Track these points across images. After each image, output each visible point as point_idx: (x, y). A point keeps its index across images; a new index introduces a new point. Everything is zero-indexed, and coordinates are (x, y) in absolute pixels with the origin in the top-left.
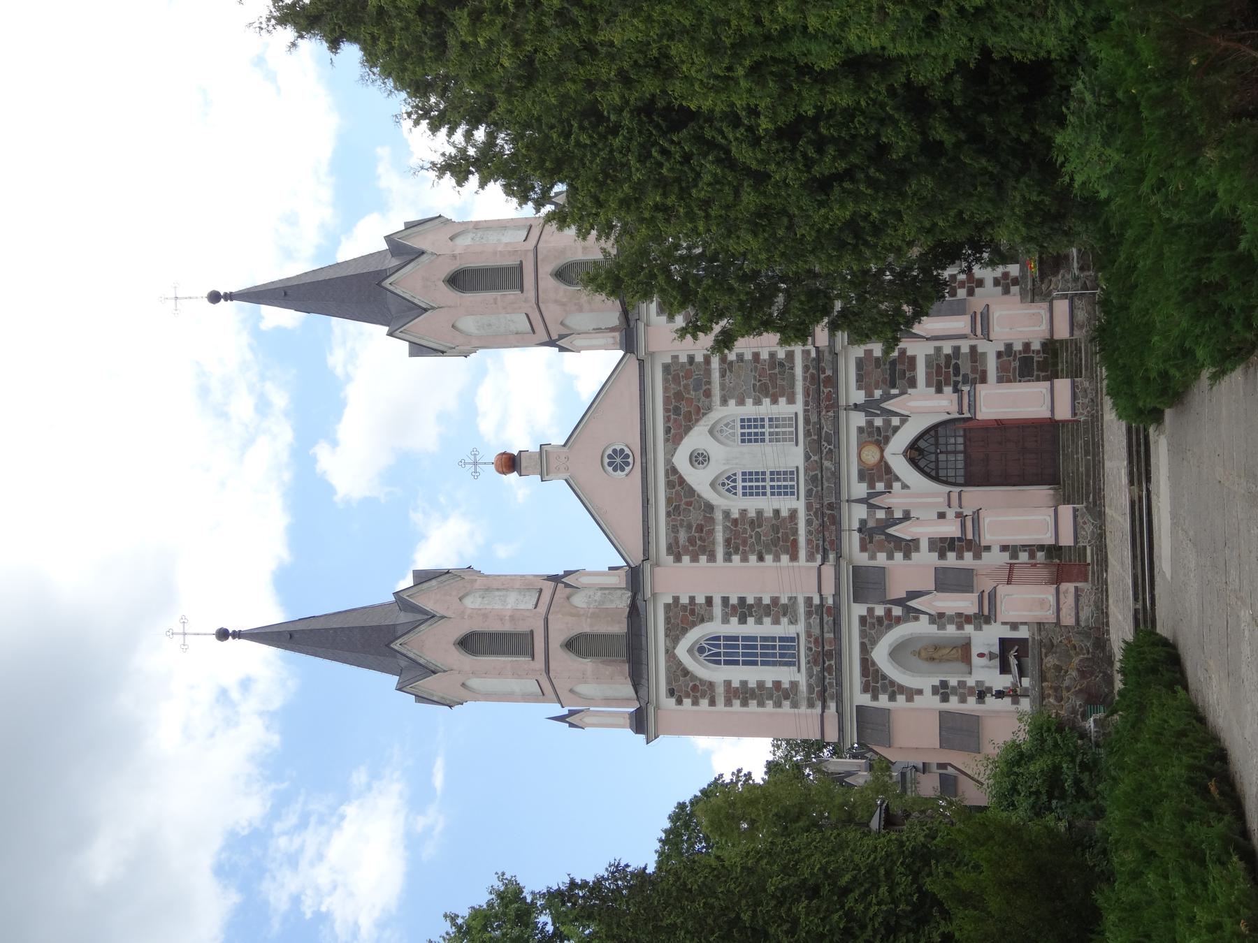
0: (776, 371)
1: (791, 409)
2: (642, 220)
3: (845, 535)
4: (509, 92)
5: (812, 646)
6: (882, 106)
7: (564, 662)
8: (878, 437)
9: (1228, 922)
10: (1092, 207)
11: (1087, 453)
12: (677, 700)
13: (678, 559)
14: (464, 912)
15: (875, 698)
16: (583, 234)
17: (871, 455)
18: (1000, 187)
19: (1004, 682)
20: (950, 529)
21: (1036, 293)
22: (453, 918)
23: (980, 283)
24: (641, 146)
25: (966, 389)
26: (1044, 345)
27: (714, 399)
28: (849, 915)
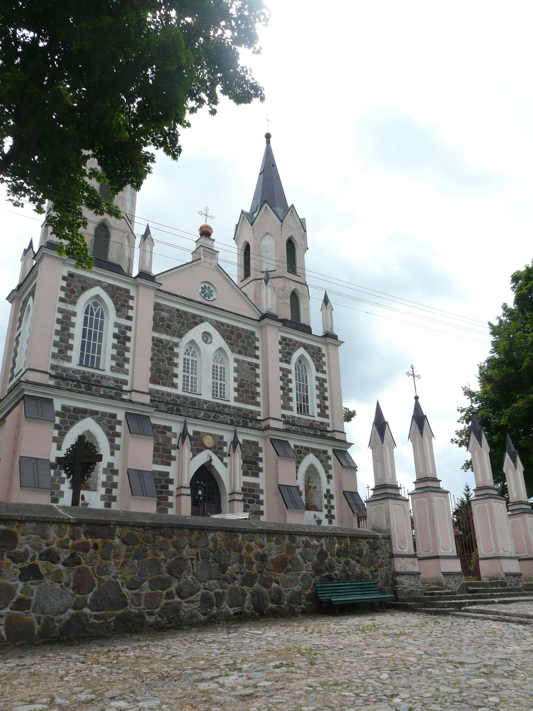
0: (250, 394)
5: (95, 378)
12: (66, 277)
27: (238, 355)
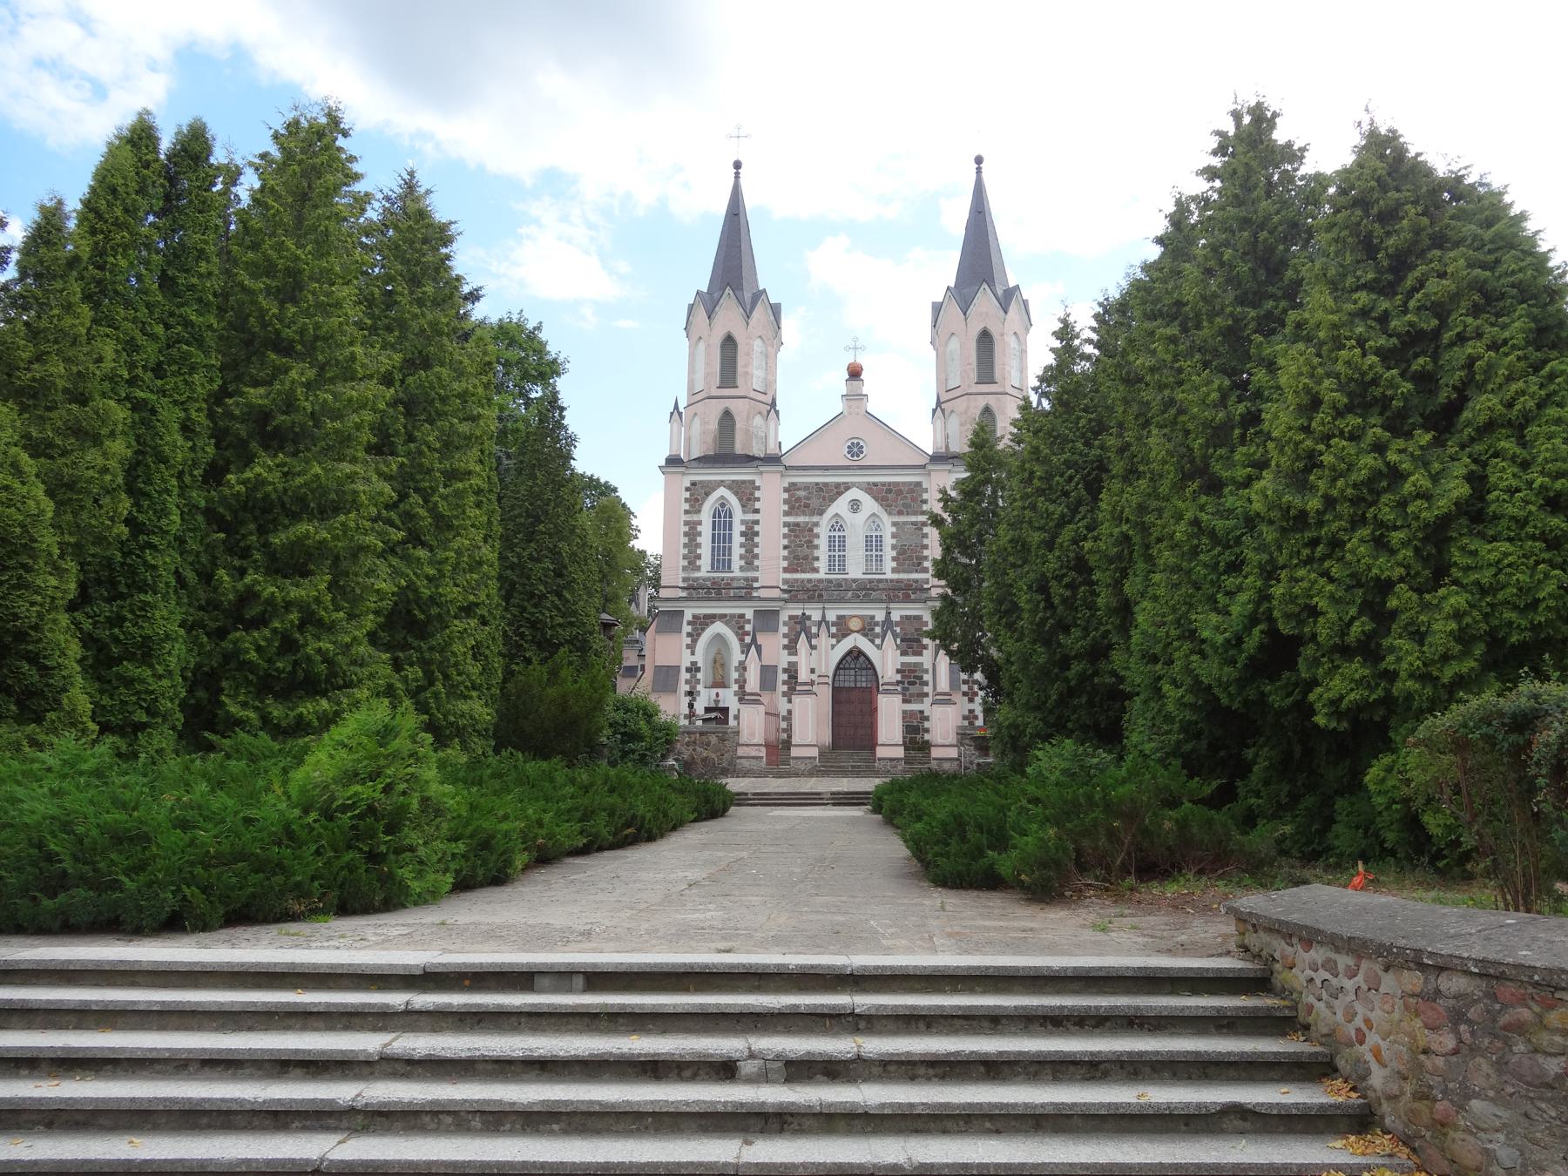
1: (888, 570)
2: (1024, 462)
3: (801, 605)
4: (1118, 366)
6: (1096, 629)
7: (714, 410)
8: (867, 630)
9: (543, 832)
10: (1019, 768)
11: (853, 767)
13: (786, 490)
14: (543, 336)
15: (689, 623)
16: (1014, 423)
17: (855, 624)
18: (1037, 708)
19: (699, 708)
20: (803, 676)
21: (963, 736)
22: (539, 328)
23: (971, 700)
24: (1076, 463)
25: (899, 688)
26: (928, 742)
28: (543, 597)
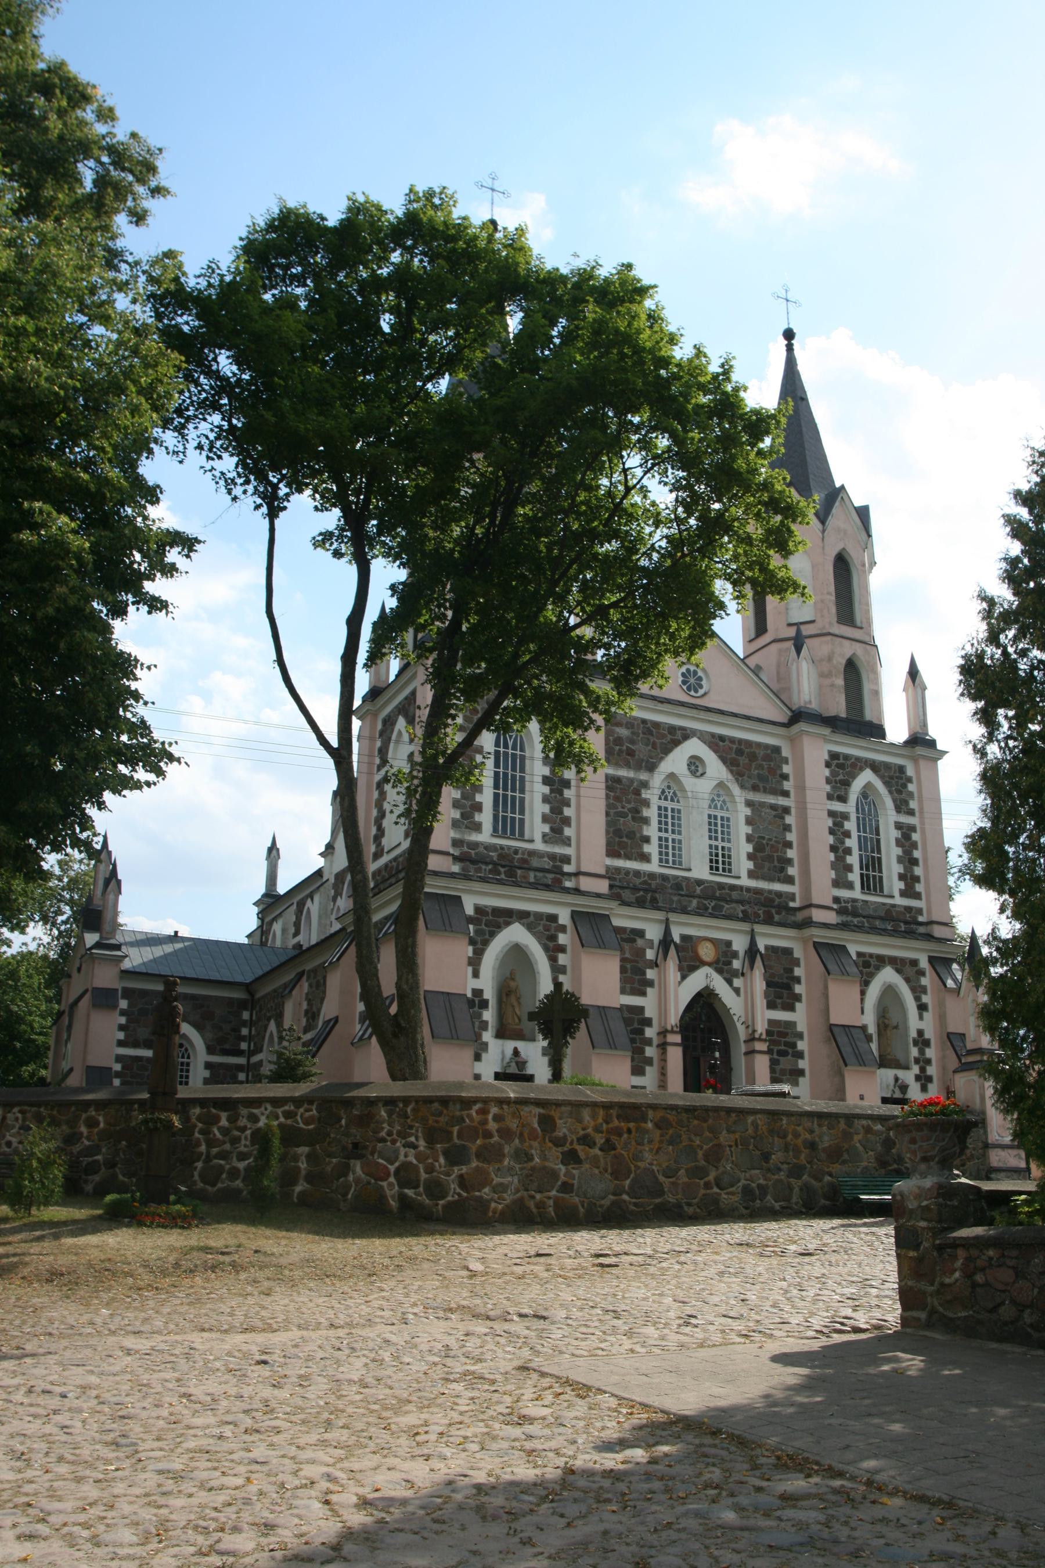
5: (519, 856)
8: (723, 964)
